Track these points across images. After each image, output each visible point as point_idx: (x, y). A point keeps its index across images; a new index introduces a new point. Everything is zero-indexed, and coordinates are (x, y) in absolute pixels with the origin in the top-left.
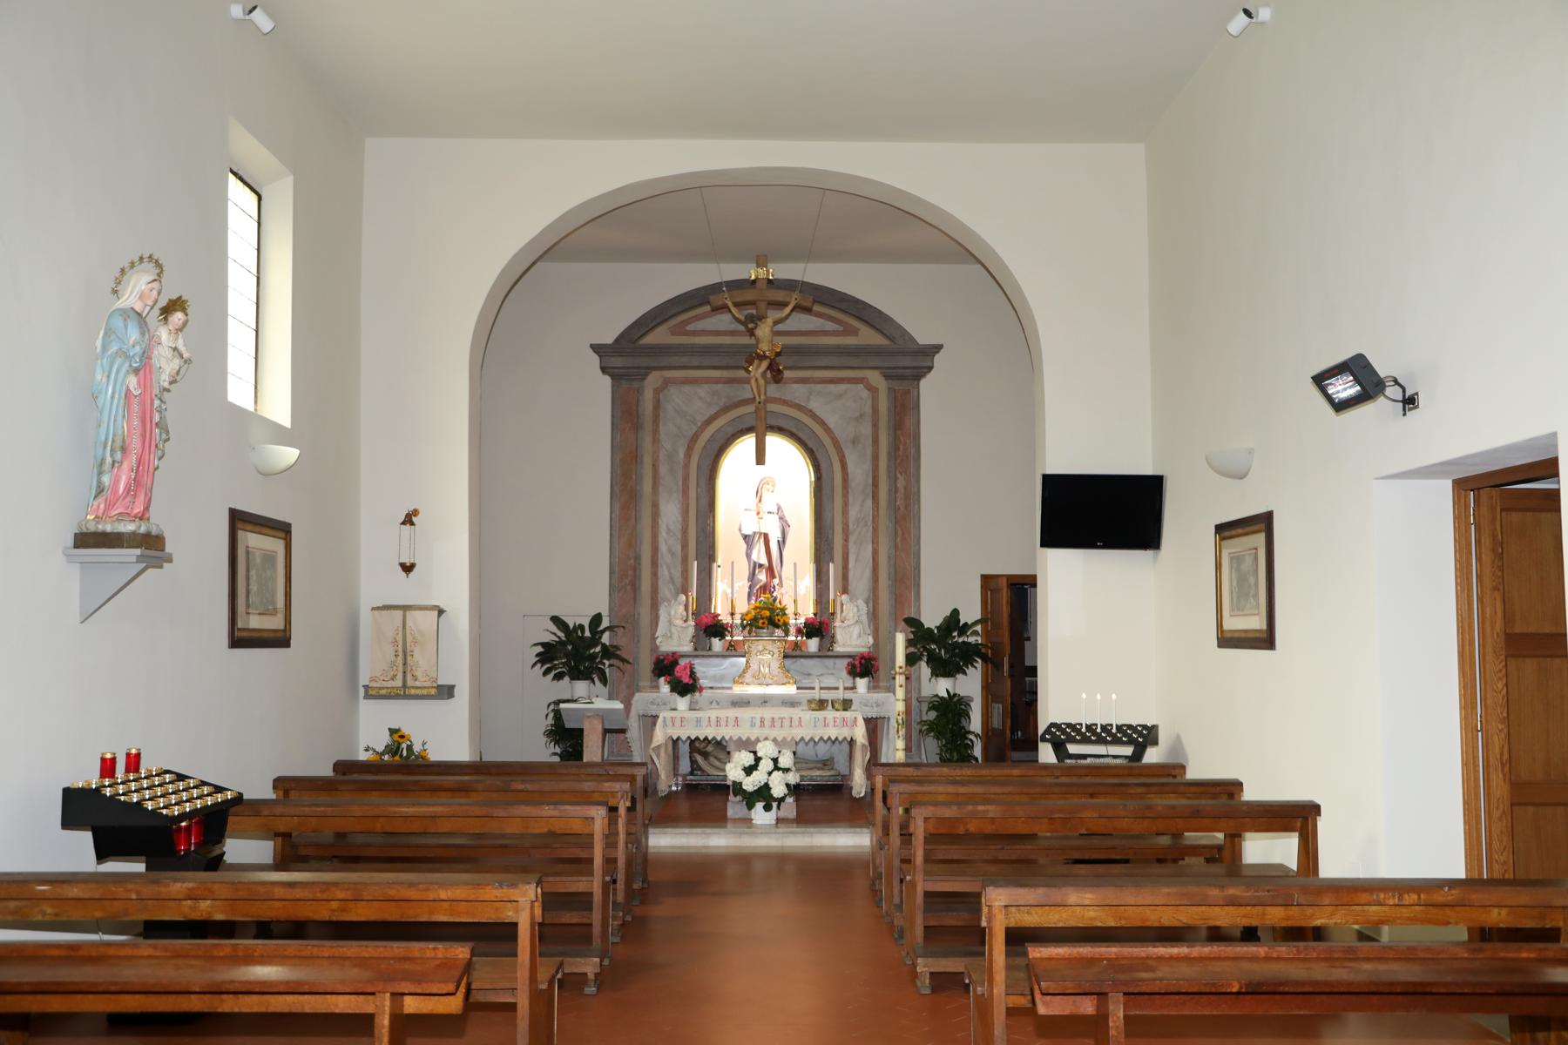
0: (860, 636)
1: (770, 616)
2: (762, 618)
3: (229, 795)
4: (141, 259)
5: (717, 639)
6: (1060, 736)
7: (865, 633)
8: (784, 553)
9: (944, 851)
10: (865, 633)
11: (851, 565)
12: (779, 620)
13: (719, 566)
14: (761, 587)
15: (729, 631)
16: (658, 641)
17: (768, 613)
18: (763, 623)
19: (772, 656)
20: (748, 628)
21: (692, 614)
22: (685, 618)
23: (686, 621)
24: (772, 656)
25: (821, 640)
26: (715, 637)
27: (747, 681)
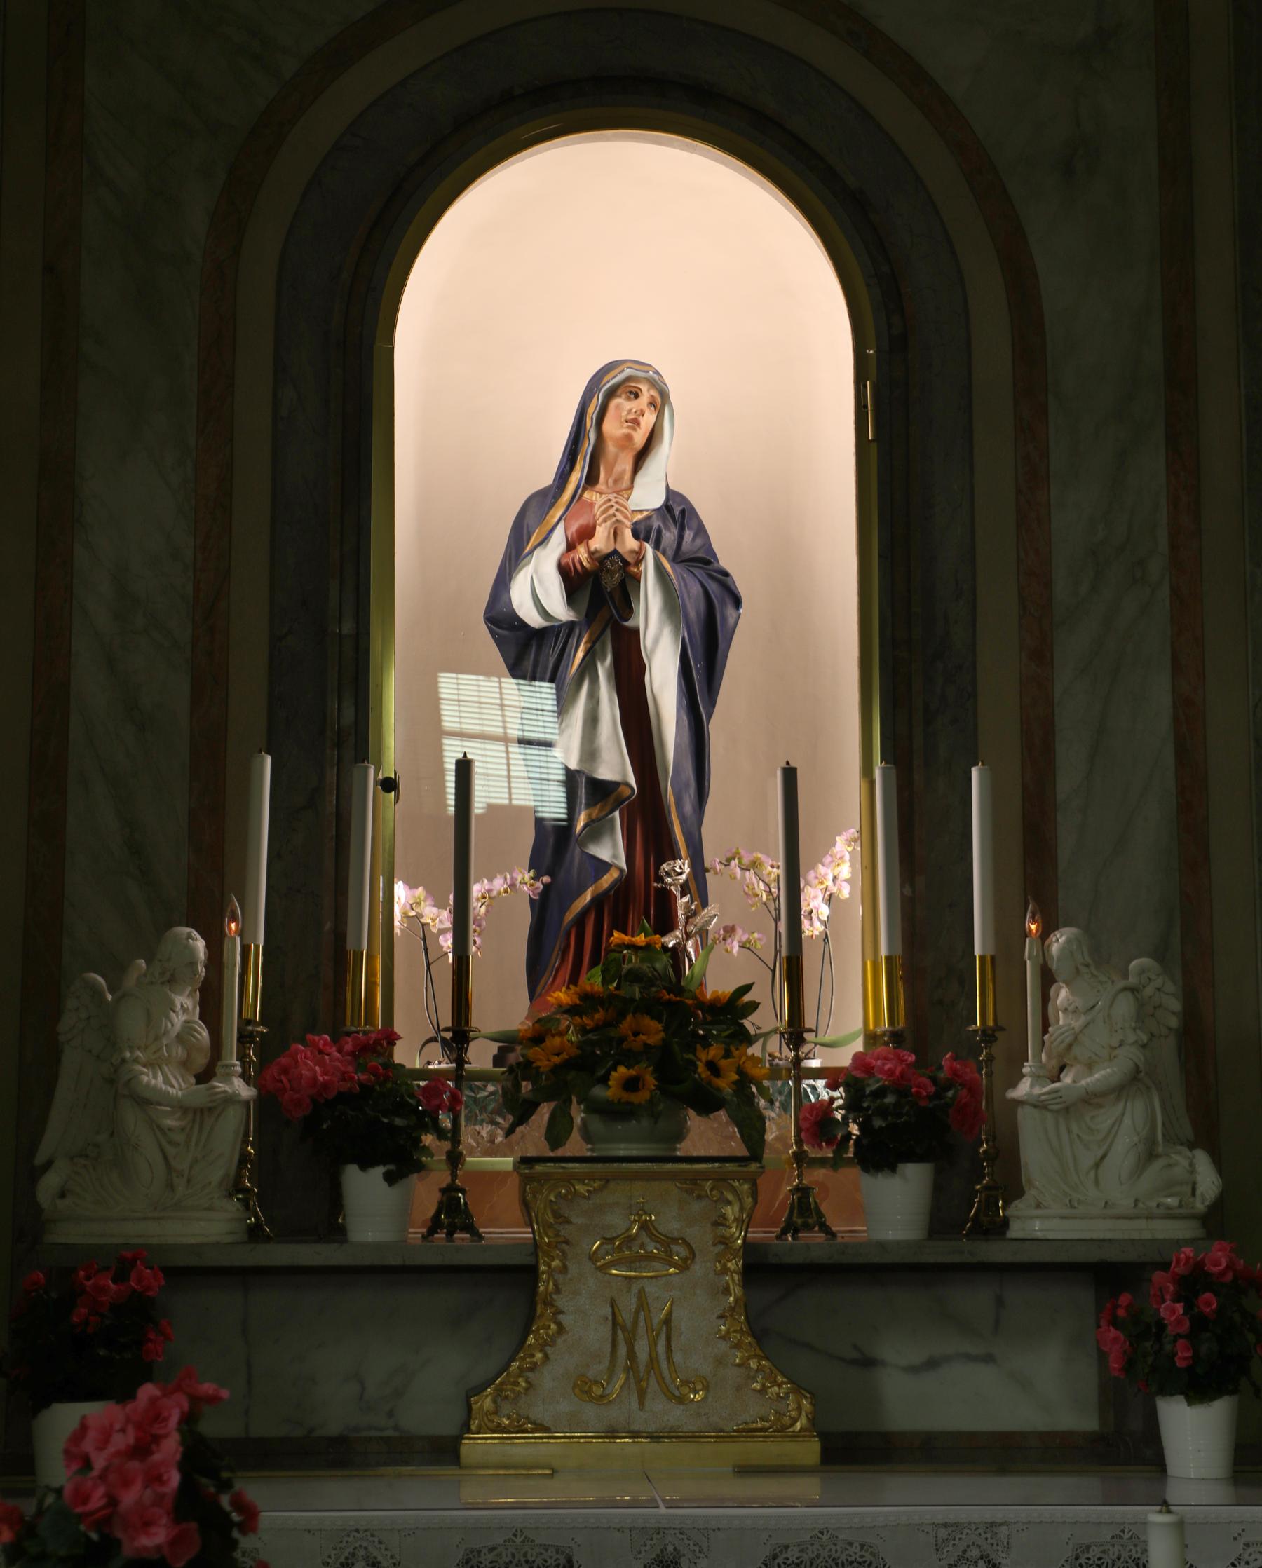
0: (1150, 1155)
1: (665, 1047)
2: (628, 1058)
3: (827, 1089)
4: (1069, 1539)
5: (379, 1171)
6: (427, 1158)
7: (1170, 1139)
8: (716, 730)
9: (356, 1023)
10: (1170, 1139)
11: (1067, 780)
12: (713, 1067)
13: (389, 785)
14: (598, 902)
15: (441, 1134)
16: (49, 1183)
17: (653, 1032)
18: (631, 1085)
19: (684, 1266)
20: (545, 1112)
21: (244, 1038)
22: (201, 1061)
23: (204, 1077)
24: (684, 1266)
25: (938, 1172)
26: (365, 1165)
27: (540, 1412)
